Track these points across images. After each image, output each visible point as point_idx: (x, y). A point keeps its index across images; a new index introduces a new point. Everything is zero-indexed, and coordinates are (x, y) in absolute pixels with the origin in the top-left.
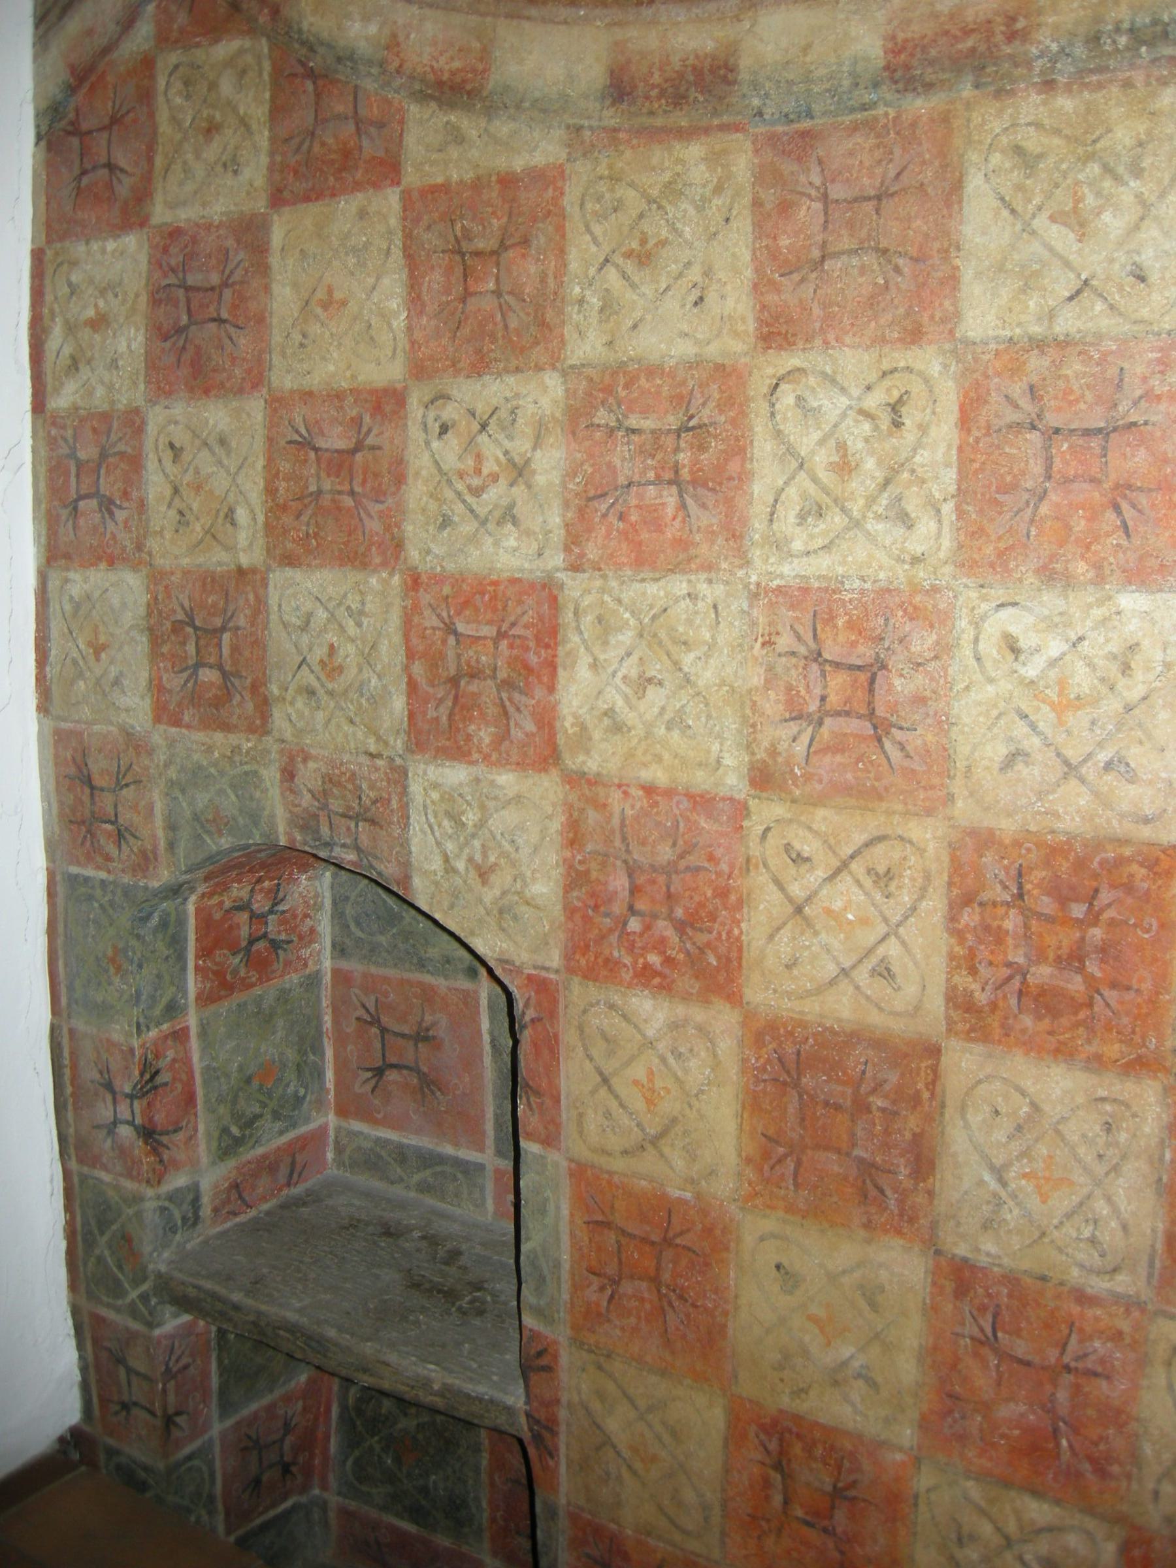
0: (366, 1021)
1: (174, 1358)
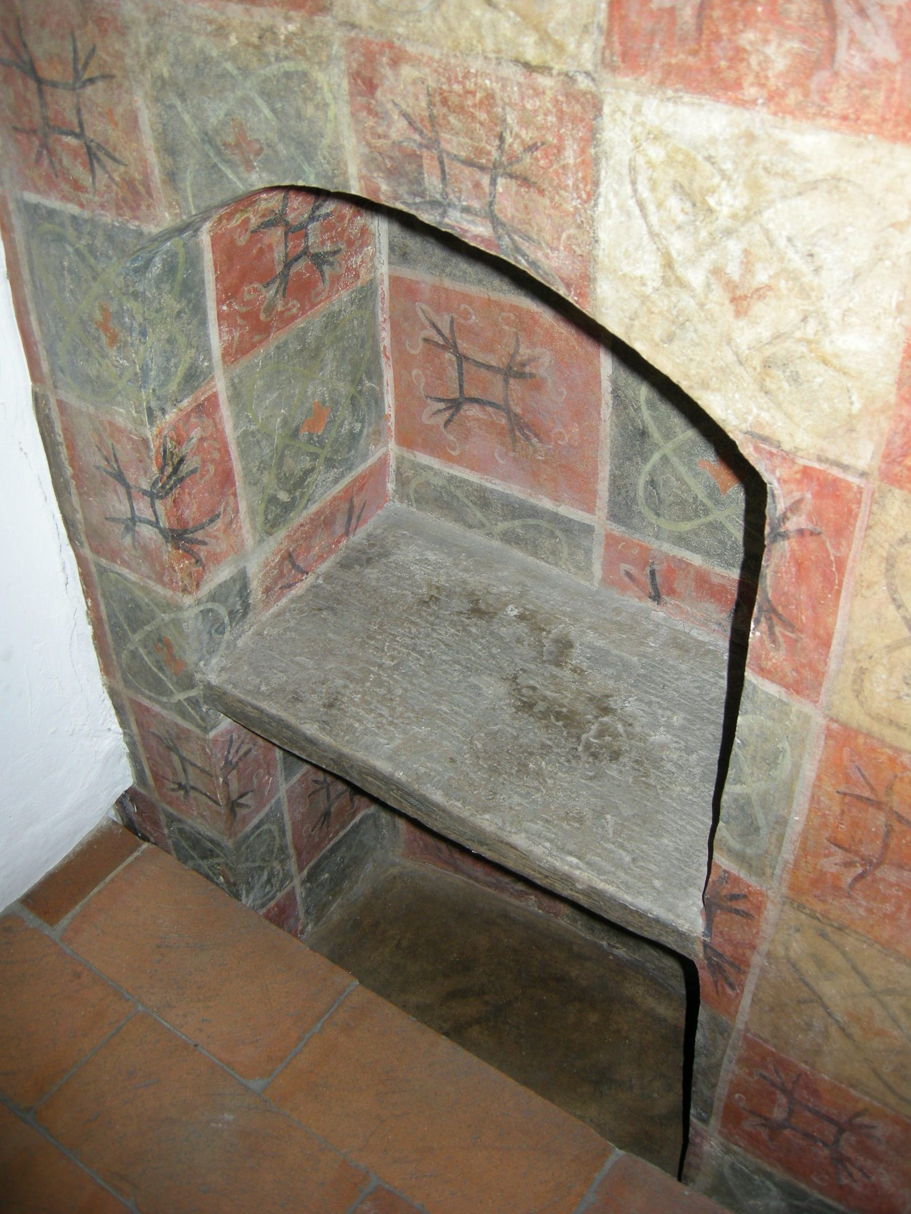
0: (437, 344)
1: (233, 751)
